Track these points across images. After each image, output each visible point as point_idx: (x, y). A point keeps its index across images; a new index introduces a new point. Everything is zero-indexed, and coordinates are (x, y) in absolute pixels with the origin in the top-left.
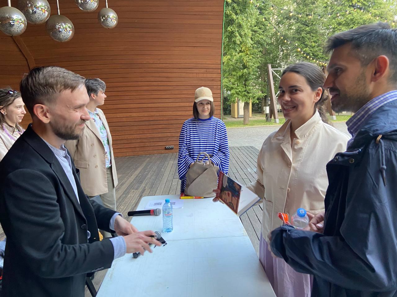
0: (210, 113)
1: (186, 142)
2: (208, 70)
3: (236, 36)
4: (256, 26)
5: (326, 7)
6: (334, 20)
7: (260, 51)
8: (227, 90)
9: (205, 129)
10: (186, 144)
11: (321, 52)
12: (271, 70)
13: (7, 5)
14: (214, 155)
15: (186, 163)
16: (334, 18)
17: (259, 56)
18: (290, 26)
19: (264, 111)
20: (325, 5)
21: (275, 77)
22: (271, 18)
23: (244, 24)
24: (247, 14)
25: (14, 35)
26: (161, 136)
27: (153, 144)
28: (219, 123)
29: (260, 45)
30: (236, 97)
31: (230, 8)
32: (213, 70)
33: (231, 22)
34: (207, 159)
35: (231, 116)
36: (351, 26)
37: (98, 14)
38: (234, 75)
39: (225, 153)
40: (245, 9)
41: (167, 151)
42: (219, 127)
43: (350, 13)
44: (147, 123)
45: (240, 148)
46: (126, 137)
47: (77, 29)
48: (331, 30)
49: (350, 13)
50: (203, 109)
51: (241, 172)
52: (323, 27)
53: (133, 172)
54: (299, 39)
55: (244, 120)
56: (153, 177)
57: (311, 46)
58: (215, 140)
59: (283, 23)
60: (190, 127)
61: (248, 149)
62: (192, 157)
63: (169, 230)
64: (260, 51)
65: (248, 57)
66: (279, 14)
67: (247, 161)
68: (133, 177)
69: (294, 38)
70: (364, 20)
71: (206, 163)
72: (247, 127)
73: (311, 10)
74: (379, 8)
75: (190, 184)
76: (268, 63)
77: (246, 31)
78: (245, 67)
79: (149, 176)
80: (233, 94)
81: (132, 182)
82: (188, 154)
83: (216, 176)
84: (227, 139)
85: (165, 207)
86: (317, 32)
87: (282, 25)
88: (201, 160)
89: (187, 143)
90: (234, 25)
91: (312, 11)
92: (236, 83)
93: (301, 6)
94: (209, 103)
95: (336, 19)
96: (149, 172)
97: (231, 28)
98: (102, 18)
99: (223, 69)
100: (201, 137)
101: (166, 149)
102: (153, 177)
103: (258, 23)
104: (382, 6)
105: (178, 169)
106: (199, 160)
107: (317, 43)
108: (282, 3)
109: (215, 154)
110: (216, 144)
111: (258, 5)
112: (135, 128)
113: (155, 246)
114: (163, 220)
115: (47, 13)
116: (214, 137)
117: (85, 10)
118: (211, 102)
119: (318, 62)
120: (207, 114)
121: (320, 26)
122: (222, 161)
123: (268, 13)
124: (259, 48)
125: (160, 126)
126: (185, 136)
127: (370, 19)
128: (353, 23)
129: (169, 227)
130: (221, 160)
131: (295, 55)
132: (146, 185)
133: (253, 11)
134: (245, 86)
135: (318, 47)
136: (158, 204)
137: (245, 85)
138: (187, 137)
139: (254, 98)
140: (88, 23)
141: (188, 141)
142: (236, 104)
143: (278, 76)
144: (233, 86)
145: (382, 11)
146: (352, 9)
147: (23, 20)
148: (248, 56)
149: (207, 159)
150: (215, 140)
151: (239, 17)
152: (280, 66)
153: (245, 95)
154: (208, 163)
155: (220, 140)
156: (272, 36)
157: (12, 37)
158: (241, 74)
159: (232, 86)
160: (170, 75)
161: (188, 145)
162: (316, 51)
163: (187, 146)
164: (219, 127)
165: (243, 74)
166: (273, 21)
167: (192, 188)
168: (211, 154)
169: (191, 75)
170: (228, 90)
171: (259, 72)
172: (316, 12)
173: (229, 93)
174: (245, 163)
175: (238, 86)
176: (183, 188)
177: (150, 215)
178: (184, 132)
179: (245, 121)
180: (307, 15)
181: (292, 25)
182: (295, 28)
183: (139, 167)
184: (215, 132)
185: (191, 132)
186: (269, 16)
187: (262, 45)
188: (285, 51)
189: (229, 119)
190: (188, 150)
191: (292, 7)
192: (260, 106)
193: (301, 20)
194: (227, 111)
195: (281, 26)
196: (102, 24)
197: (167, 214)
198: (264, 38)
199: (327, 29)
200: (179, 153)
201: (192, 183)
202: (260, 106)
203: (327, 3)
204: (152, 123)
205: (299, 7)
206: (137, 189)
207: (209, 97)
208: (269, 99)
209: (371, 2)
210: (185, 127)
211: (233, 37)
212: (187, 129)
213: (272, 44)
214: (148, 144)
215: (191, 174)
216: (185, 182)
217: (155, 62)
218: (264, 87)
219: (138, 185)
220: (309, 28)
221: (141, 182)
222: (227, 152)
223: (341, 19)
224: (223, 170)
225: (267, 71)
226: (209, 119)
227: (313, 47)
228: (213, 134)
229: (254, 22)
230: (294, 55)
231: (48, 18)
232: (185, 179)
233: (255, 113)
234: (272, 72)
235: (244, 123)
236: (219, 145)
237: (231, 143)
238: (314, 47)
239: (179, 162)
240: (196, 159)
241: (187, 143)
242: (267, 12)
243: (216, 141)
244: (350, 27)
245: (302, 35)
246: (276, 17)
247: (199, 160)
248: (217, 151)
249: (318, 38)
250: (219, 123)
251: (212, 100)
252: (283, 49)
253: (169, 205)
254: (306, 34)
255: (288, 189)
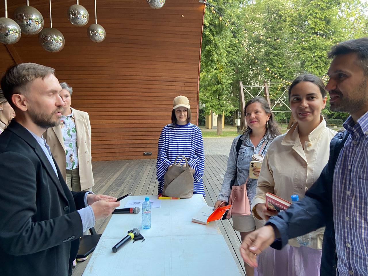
0: (187, 119)
1: (164, 146)
2: (186, 83)
3: (213, 55)
4: (229, 47)
5: (291, 34)
6: (298, 45)
7: (233, 70)
8: (202, 103)
9: (183, 133)
10: (165, 148)
11: (287, 73)
12: (242, 87)
13: (4, 16)
14: (190, 158)
15: (164, 165)
16: (299, 44)
17: (231, 74)
18: (260, 49)
19: (235, 124)
20: (291, 32)
21: (245, 93)
22: (243, 41)
23: (220, 44)
24: (223, 36)
25: (8, 44)
26: (140, 142)
27: (132, 150)
28: (196, 129)
29: (233, 64)
30: (210, 110)
31: (208, 30)
32: (190, 84)
33: (208, 42)
34: (185, 161)
35: (205, 127)
36: (314, 51)
37: (88, 29)
38: (209, 90)
39: (201, 157)
40: (221, 31)
41: (145, 157)
42: (195, 132)
43: (313, 40)
44: (128, 130)
45: (213, 156)
46: (108, 142)
47: (67, 41)
48: (296, 54)
49: (313, 40)
50: (180, 115)
51: (214, 178)
52: (288, 51)
53: (112, 175)
54: (267, 61)
55: (218, 132)
56: (132, 181)
57: (278, 67)
58: (192, 145)
59: (253, 46)
60: (168, 132)
61: (221, 158)
62: (170, 160)
63: (147, 228)
64: (233, 70)
65: (222, 75)
66: (251, 37)
67: (220, 168)
68: (113, 180)
69: (263, 59)
70: (325, 46)
71: (183, 166)
72: (220, 137)
73: (278, 36)
74: (339, 36)
75: (167, 185)
76: (240, 81)
77: (222, 50)
78: (219, 83)
79: (128, 179)
80: (208, 107)
81: (111, 185)
82: (166, 157)
83: (192, 178)
84: (202, 144)
85: (144, 204)
86: (283, 55)
87: (252, 48)
88: (179, 162)
89: (166, 146)
90: (211, 45)
91: (279, 37)
92: (211, 97)
93: (269, 32)
94: (186, 110)
95: (301, 44)
96: (127, 176)
97: (209, 47)
98: (91, 33)
99: (199, 84)
100: (179, 140)
101: (144, 155)
102: (132, 181)
103: (231, 45)
104: (342, 34)
105: (157, 171)
106: (177, 162)
107: (283, 64)
108: (253, 29)
109: (191, 157)
110: (192, 148)
111: (232, 28)
112: (116, 134)
113: (134, 242)
114: (141, 218)
115: (40, 26)
116: (191, 142)
117: (75, 25)
118: (187, 109)
119: (284, 80)
120: (184, 120)
121: (287, 50)
122: (198, 164)
123: (240, 37)
124: (232, 66)
125: (140, 133)
126: (164, 140)
127: (331, 45)
128: (316, 48)
129: (146, 225)
130: (197, 163)
131: (264, 75)
132: (125, 187)
133: (228, 34)
134: (218, 100)
135: (284, 68)
136: (137, 203)
137: (219, 99)
138: (166, 141)
139: (227, 111)
140: (78, 36)
141: (166, 144)
142: (210, 116)
143: (249, 92)
144: (208, 100)
145: (341, 39)
146: (315, 36)
147: (18, 30)
148: (222, 73)
149: (185, 161)
150: (192, 145)
151: (216, 38)
152: (251, 85)
153: (218, 109)
154: (185, 166)
155: (196, 144)
156: (244, 57)
157: (5, 45)
158: (215, 89)
159: (207, 99)
160: (150, 86)
161: (166, 148)
162: (283, 72)
163: (166, 149)
164: (195, 132)
165: (217, 89)
166: (245, 44)
167: (169, 190)
168: (187, 157)
169: (170, 87)
170: (204, 103)
171: (232, 89)
172: (283, 37)
173: (204, 105)
174: (218, 170)
175: (212, 100)
176: (160, 189)
177: (129, 213)
178: (163, 136)
179: (218, 132)
180: (275, 40)
181: (262, 48)
182: (264, 51)
183: (118, 171)
184: (192, 136)
185: (170, 134)
186: (241, 39)
187: (234, 64)
188: (255, 71)
189: (203, 130)
190: (166, 153)
191: (262, 32)
192: (232, 119)
193: (269, 44)
194: (202, 122)
195: (252, 49)
196: (91, 38)
197: (146, 211)
198: (237, 58)
199: (293, 52)
200: (158, 156)
201: (170, 184)
202: (232, 119)
203: (293, 30)
204: (132, 130)
205: (268, 32)
206: (115, 191)
207: (186, 104)
208: (240, 112)
209: (331, 30)
210: (164, 132)
211: (211, 56)
212: (166, 134)
213: (243, 64)
214: (127, 150)
215: (169, 176)
216: (162, 186)
217: (138, 75)
218: (235, 102)
219: (117, 188)
220: (277, 51)
221: (120, 185)
222: (203, 155)
223: (305, 44)
224: (199, 173)
225: (239, 88)
226: (187, 125)
227: (280, 68)
228: (190, 137)
229: (228, 43)
230: (264, 74)
231: (41, 31)
232: (163, 181)
233: (227, 125)
234: (244, 89)
235: (217, 134)
236: (195, 149)
237: (206, 151)
238: (281, 68)
239: (158, 165)
240: (174, 161)
241: (166, 146)
242: (239, 36)
243: (192, 146)
244: (313, 52)
245: (270, 57)
246: (247, 40)
247: (177, 162)
248: (193, 155)
249: (285, 60)
250: (196, 129)
251: (188, 107)
252: (253, 69)
253: (148, 202)
254: (274, 57)
255: (288, 110)
